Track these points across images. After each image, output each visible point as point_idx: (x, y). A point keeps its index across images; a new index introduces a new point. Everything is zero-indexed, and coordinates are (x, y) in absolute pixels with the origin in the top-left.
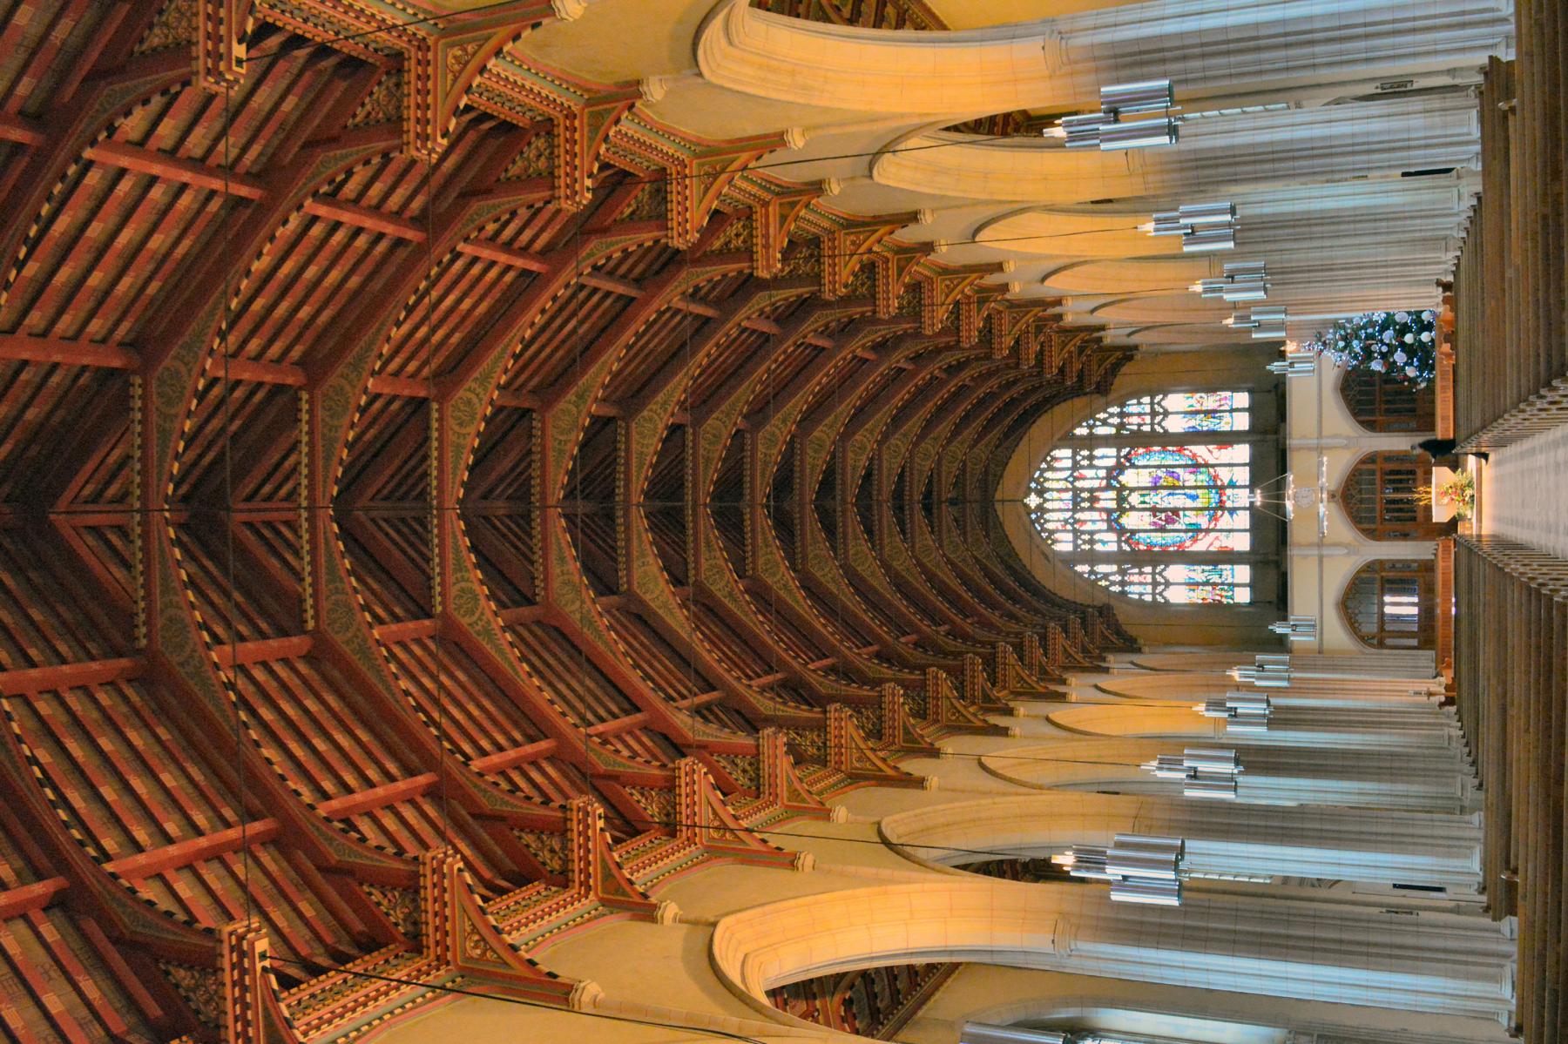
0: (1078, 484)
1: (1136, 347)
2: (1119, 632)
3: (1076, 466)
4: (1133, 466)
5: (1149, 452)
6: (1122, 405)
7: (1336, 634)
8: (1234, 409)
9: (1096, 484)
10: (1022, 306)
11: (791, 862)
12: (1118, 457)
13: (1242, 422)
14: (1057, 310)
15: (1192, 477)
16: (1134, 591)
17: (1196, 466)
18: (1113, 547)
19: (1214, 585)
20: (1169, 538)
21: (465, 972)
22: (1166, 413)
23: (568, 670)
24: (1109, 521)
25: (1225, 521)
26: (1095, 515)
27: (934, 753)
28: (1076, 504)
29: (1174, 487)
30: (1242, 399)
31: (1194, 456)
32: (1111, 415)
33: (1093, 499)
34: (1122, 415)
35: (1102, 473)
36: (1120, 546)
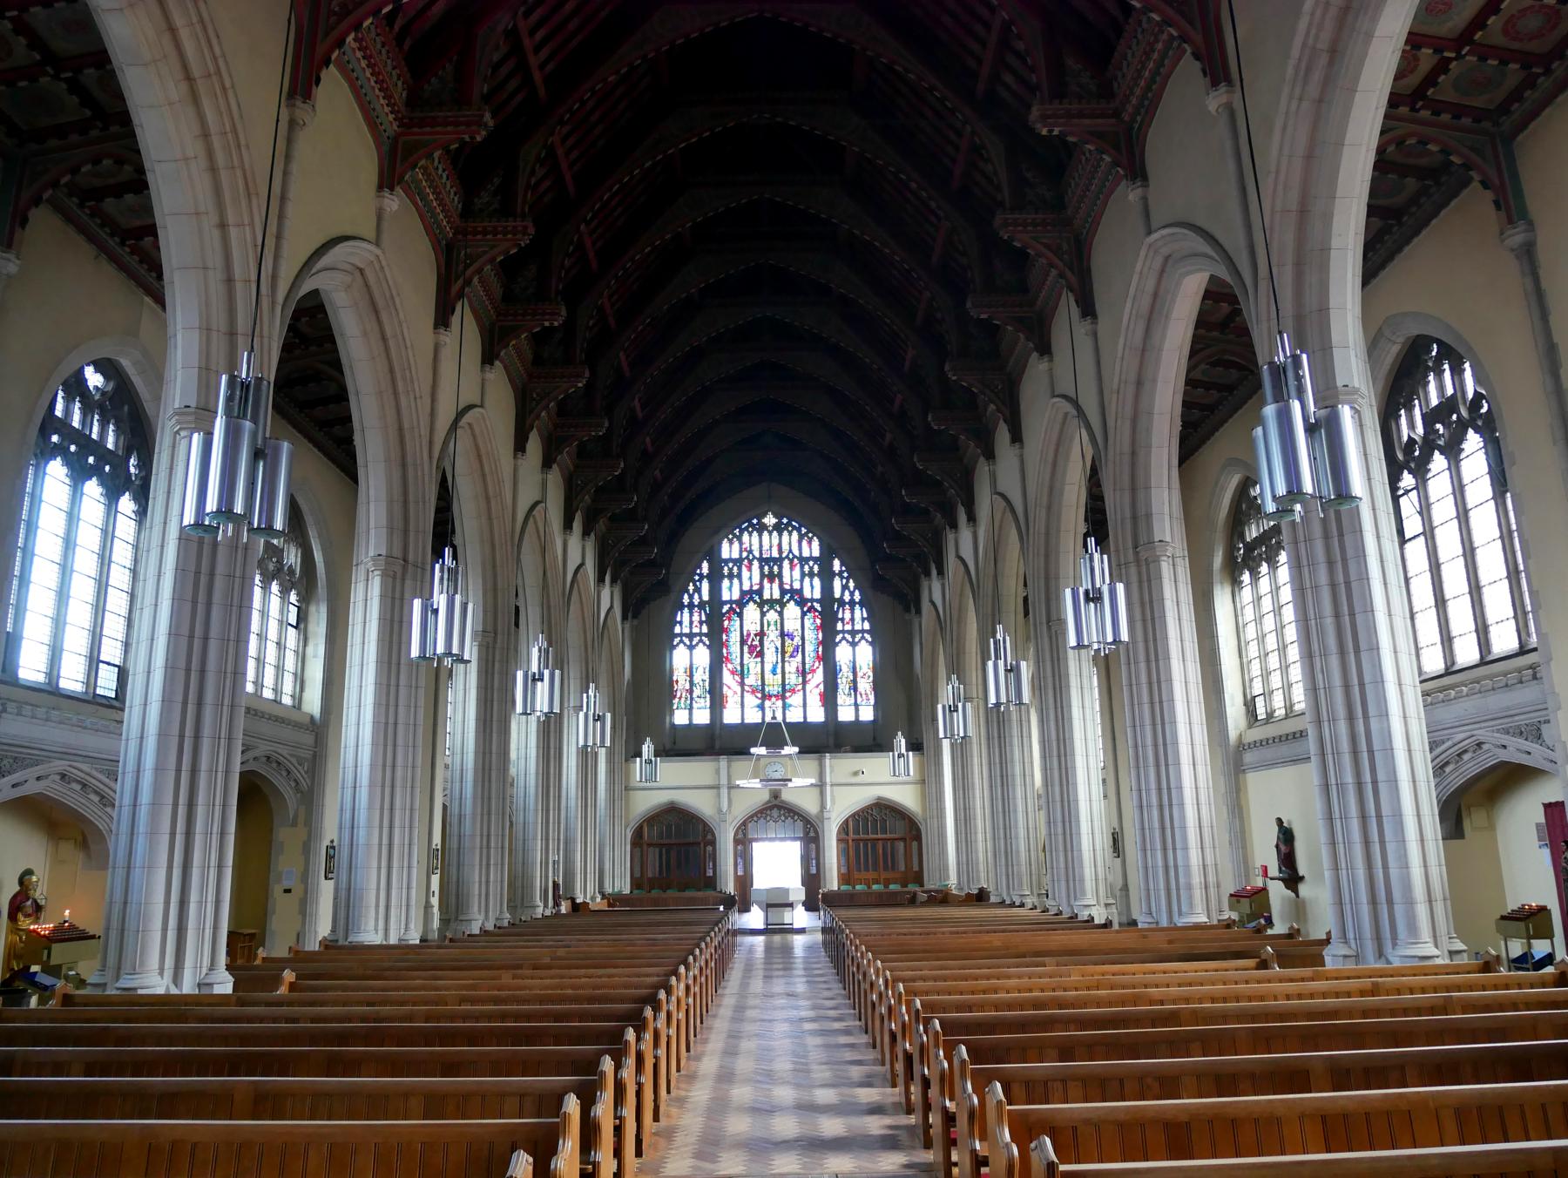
0: (786, 564)
1: (919, 611)
4: (804, 614)
6: (861, 604)
7: (646, 802)
8: (857, 708)
9: (786, 579)
11: (442, 319)
12: (812, 600)
13: (845, 714)
14: (934, 572)
15: (793, 669)
18: (726, 596)
19: (691, 691)
24: (751, 592)
25: (752, 701)
29: (784, 653)
30: (867, 714)
31: (813, 671)
32: (852, 594)
33: (772, 578)
35: (797, 585)
36: (726, 602)
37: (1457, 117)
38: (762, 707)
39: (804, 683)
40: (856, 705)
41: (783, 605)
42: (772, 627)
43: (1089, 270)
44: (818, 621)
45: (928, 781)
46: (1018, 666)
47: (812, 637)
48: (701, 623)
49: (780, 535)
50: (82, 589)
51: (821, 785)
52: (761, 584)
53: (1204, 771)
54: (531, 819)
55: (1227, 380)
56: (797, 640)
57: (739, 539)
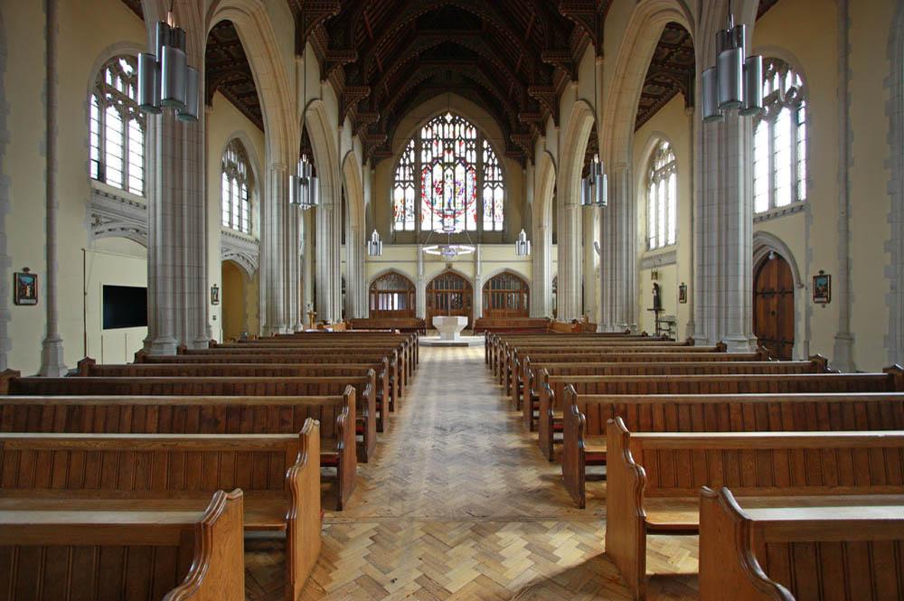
0: (457, 142)
3: (467, 141)
4: (466, 171)
5: (473, 179)
6: (498, 166)
7: (376, 270)
8: (493, 223)
9: (457, 151)
11: (299, 51)
12: (471, 164)
13: (487, 226)
18: (424, 160)
19: (404, 212)
22: (493, 188)
24: (438, 158)
25: (437, 218)
28: (449, 139)
29: (455, 192)
30: (499, 227)
32: (493, 161)
33: (449, 150)
34: (493, 166)
35: (463, 155)
38: (442, 221)
39: (466, 209)
40: (494, 222)
41: (455, 166)
42: (449, 178)
43: (603, 28)
44: (474, 175)
47: (471, 183)
48: (410, 175)
49: (454, 126)
52: (443, 154)
54: (324, 276)
55: (672, 74)
56: (463, 186)
57: (432, 128)
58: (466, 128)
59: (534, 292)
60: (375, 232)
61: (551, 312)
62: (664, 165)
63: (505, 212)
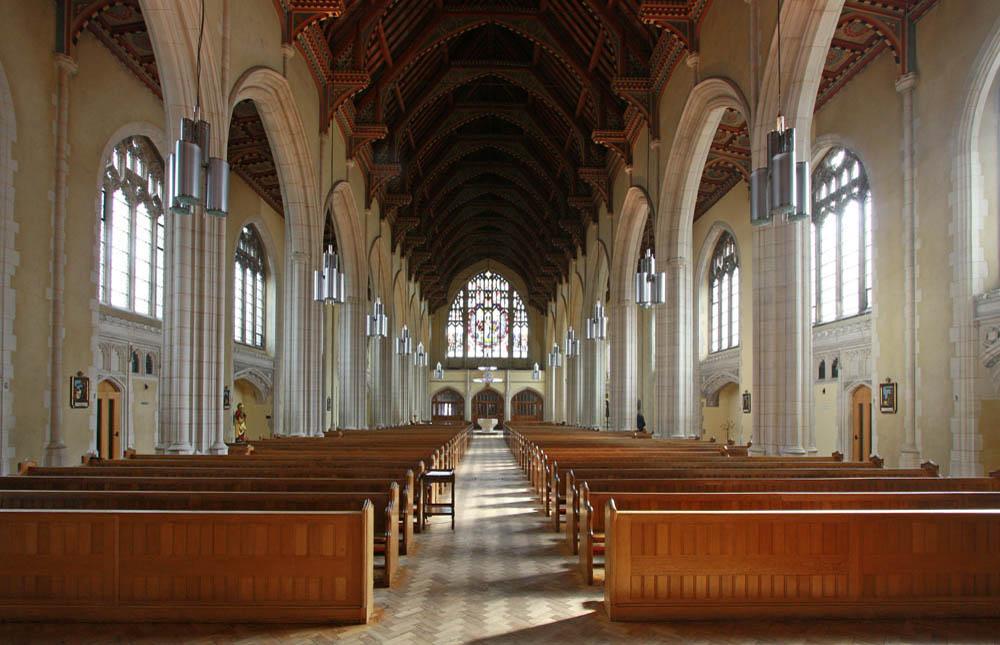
0: (494, 293)
1: (547, 315)
2: (437, 307)
3: (502, 292)
7: (437, 387)
8: (521, 352)
9: (494, 299)
10: (555, 290)
13: (516, 355)
14: (564, 280)
16: (453, 313)
17: (500, 337)
18: (469, 306)
20: (473, 327)
21: (289, 13)
22: (520, 327)
23: (411, 23)
24: (480, 304)
25: (479, 348)
26: (482, 299)
27: (382, 217)
28: (487, 291)
30: (525, 355)
33: (488, 298)
34: (521, 310)
35: (498, 302)
37: (740, 153)
45: (547, 382)
46: (659, 278)
47: (504, 323)
50: (249, 308)
51: (505, 382)
53: (690, 383)
58: (501, 282)
59: (546, 404)
60: (421, 345)
61: (635, 422)
62: (833, 189)
63: (529, 344)
